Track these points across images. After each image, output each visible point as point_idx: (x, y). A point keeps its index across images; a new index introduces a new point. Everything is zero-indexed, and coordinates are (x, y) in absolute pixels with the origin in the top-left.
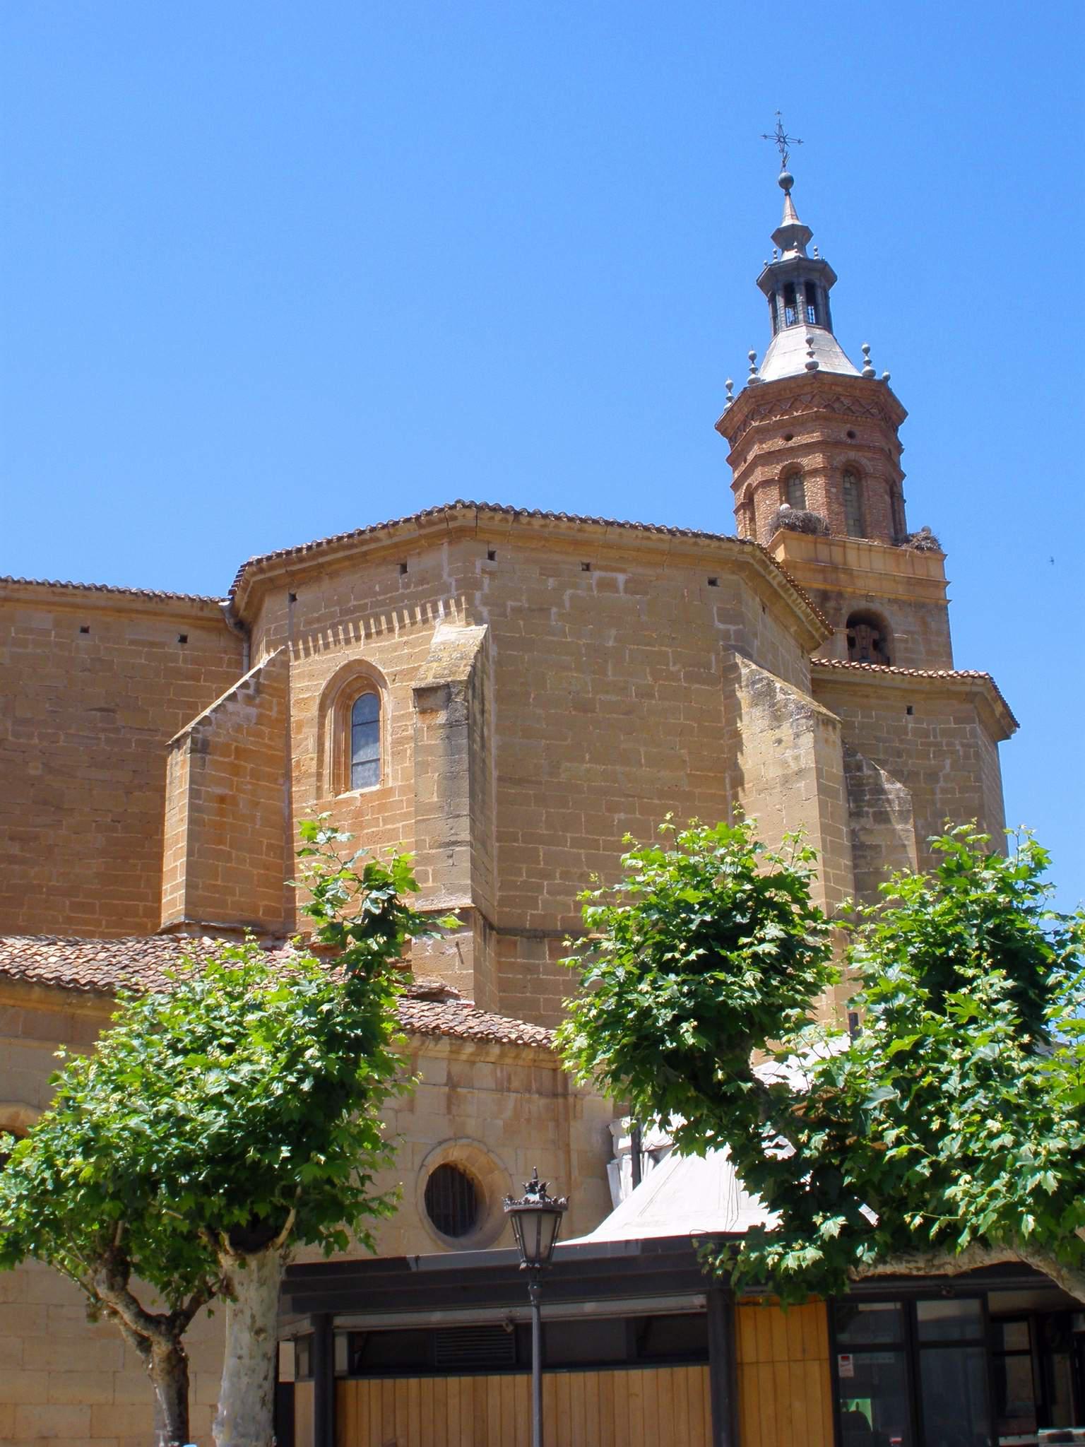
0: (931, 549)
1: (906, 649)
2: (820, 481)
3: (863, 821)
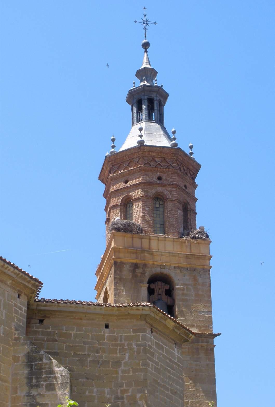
0: (204, 237)
1: (183, 294)
3: (39, 390)
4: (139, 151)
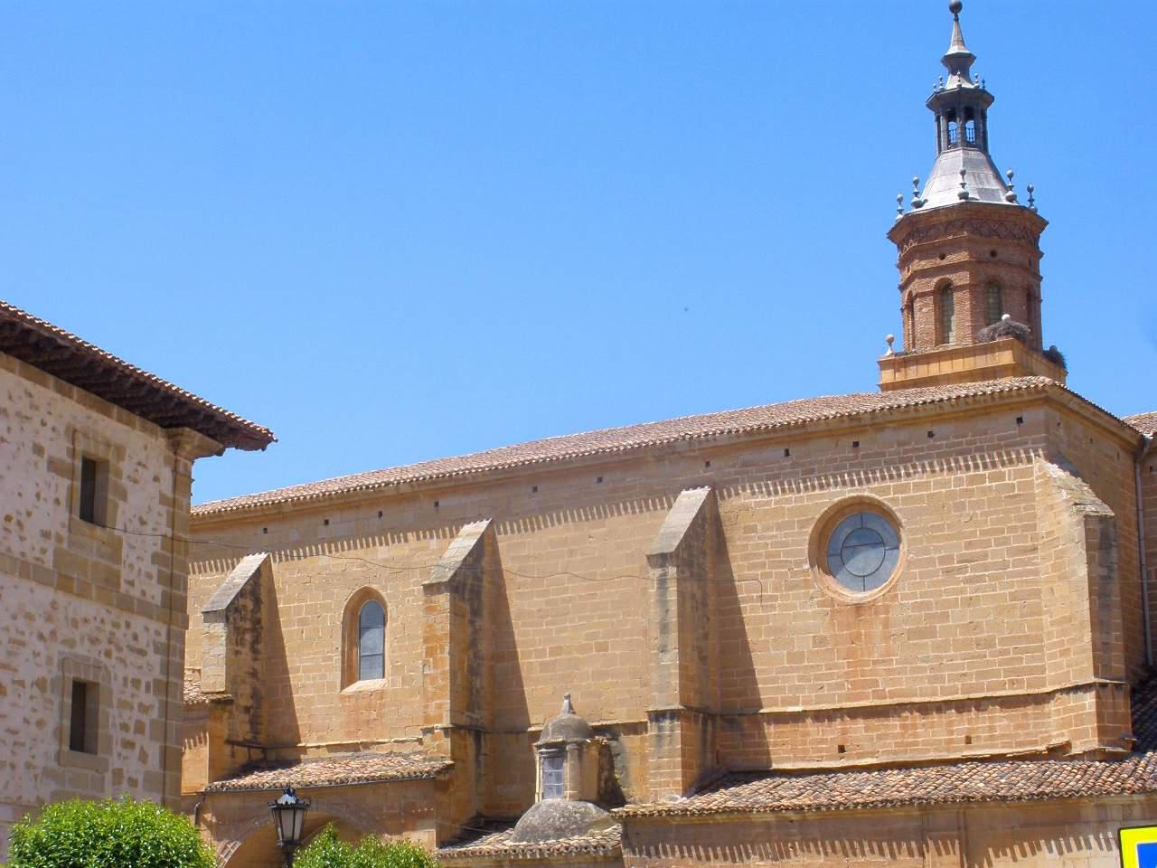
2: (966, 295)
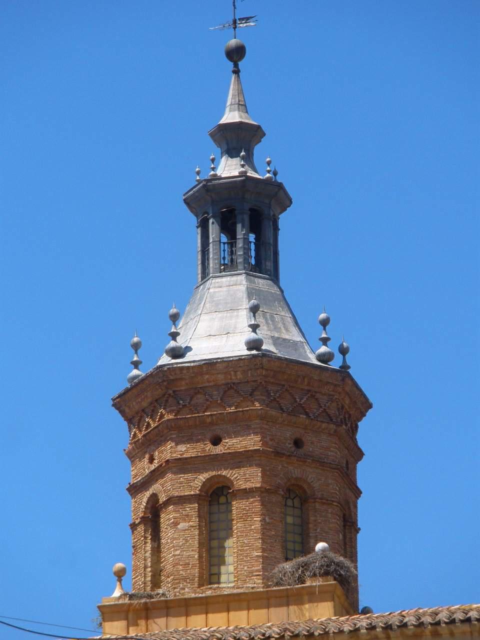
2: (254, 505)
4: (339, 386)
